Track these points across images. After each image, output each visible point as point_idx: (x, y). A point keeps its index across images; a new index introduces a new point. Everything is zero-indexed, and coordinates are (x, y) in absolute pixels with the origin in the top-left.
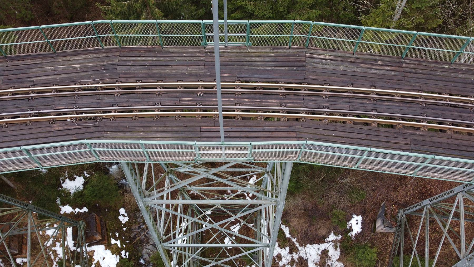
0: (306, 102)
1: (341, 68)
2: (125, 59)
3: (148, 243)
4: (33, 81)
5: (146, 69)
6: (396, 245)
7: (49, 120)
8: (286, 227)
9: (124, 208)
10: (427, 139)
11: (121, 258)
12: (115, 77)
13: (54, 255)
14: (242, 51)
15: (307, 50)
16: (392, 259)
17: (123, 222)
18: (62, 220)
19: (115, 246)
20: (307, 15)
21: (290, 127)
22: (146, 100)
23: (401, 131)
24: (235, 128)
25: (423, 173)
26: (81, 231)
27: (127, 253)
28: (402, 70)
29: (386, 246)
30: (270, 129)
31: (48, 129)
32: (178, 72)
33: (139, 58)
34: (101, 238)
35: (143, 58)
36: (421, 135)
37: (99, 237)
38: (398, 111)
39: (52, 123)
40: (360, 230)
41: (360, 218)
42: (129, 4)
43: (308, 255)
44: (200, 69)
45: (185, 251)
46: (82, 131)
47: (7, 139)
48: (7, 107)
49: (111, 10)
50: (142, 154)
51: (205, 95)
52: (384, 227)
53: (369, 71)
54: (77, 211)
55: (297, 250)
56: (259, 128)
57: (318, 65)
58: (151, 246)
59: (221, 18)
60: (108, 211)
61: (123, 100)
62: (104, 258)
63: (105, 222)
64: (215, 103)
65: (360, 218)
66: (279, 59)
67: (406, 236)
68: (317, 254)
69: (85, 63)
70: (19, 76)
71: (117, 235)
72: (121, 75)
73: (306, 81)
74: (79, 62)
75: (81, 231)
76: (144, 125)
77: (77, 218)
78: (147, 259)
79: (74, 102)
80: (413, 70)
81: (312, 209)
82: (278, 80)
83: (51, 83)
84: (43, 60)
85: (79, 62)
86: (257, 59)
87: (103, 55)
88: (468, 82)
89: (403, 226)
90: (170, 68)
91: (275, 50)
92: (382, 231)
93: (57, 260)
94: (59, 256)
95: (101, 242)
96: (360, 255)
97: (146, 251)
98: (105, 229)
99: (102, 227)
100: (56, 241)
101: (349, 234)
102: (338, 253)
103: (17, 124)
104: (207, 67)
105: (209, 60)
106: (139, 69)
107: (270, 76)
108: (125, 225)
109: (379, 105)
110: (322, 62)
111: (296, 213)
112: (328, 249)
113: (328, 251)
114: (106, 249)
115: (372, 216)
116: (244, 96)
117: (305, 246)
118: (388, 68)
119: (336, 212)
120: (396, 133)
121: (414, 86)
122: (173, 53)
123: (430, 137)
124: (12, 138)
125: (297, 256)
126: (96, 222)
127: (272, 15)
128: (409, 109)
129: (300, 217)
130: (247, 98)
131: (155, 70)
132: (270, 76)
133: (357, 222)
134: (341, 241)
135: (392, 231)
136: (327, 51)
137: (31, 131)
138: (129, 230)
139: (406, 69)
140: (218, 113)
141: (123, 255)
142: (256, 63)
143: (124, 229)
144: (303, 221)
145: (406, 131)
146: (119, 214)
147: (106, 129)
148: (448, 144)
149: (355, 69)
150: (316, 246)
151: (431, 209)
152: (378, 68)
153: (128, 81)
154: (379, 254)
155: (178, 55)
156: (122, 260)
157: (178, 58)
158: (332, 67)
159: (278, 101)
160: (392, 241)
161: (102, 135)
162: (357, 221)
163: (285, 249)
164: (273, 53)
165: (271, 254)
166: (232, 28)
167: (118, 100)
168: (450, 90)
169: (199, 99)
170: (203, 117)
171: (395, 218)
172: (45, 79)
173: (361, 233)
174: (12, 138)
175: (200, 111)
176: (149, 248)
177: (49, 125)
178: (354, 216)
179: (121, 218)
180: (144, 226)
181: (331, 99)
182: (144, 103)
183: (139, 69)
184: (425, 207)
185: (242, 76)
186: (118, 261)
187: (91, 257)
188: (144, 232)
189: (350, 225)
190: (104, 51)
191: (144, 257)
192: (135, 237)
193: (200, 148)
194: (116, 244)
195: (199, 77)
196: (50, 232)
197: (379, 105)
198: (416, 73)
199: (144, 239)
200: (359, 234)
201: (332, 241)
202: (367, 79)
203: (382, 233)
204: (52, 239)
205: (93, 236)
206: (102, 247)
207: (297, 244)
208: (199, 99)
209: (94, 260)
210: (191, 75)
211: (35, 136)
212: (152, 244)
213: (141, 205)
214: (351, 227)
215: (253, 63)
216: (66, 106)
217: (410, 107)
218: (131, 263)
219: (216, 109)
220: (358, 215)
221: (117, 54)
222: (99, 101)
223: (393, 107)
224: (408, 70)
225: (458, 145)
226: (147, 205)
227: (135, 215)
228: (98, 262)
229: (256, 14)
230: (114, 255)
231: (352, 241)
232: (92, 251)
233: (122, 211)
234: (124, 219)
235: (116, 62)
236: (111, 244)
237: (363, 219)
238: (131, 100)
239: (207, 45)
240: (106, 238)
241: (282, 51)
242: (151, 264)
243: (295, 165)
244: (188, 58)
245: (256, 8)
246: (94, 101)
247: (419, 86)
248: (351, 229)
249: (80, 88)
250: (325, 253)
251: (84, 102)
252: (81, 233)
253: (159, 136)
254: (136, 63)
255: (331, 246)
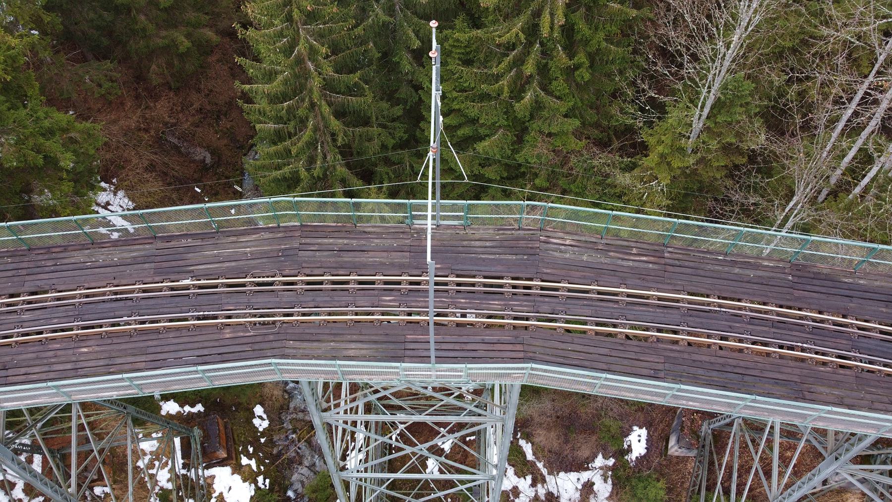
0: (537, 304)
1: (585, 258)
2: (308, 241)
3: (301, 464)
4: (192, 271)
5: (335, 256)
6: (697, 477)
7: (216, 325)
8: (527, 443)
9: (262, 405)
10: (686, 356)
11: (258, 489)
12: (296, 266)
13: (151, 483)
14: (458, 232)
15: (543, 233)
16: (691, 498)
17: (261, 429)
18: (170, 428)
19: (247, 469)
20: (559, 125)
21: (517, 337)
22: (336, 299)
23: (654, 345)
24: (448, 338)
25: (675, 402)
26: (196, 443)
27: (268, 481)
28: (663, 261)
29: (682, 478)
30: (493, 339)
31: (216, 337)
32: (375, 261)
33: (326, 241)
34: (226, 456)
35: (331, 241)
36: (678, 351)
37: (223, 454)
38: (652, 318)
39: (221, 329)
40: (643, 452)
41: (644, 432)
42: (289, 107)
43: (560, 490)
44: (404, 257)
45: (365, 482)
46: (259, 339)
47: (166, 349)
48: (163, 306)
49: (259, 110)
50: (336, 373)
51: (411, 294)
52: (680, 448)
53: (620, 262)
54: (187, 411)
55: (544, 481)
56: (478, 339)
57: (555, 253)
58: (306, 469)
59: (436, 284)
60: (236, 410)
61: (309, 299)
62: (230, 488)
63: (232, 429)
64: (423, 304)
65: (644, 432)
66: (506, 244)
67: (711, 463)
68: (577, 488)
69: (257, 246)
70: (174, 264)
71: (251, 450)
72: (304, 265)
73: (539, 275)
74: (249, 244)
75: (196, 443)
76: (335, 332)
77: (189, 423)
78: (300, 491)
79: (246, 300)
80: (677, 262)
81: (570, 415)
82: (503, 274)
83: (216, 274)
84: (202, 241)
85: (249, 244)
86: (478, 243)
87: (279, 235)
88: (745, 280)
89: (707, 448)
90: (365, 254)
91: (501, 232)
92: (676, 454)
93: (157, 491)
94: (160, 484)
95: (225, 462)
96: (639, 492)
97: (300, 476)
98: (232, 441)
99: (227, 437)
100: (155, 460)
101: (626, 457)
102: (609, 487)
103: (178, 329)
104: (412, 254)
105: (416, 244)
106: (327, 256)
107: (493, 269)
108: (263, 434)
109: (629, 309)
110: (560, 249)
111: (543, 422)
112: (593, 480)
113: (593, 484)
114: (233, 474)
115: (663, 430)
116: (459, 295)
117: (558, 474)
118: (644, 258)
119: (607, 421)
120: (648, 348)
121: (675, 285)
122: (369, 233)
123: (689, 353)
124: (172, 348)
125: (544, 492)
126: (219, 429)
127: (506, 123)
128: (667, 316)
129: (549, 429)
130: (463, 299)
131: (347, 258)
132: (493, 269)
133: (639, 438)
134: (613, 468)
135: (693, 453)
136: (567, 233)
137: (196, 339)
138: (271, 442)
139: (668, 261)
140: (428, 318)
141: (260, 484)
142: (475, 249)
143: (263, 440)
144: (553, 434)
145: (660, 345)
146: (253, 415)
147: (288, 337)
148: (711, 363)
149: (603, 260)
150: (573, 476)
151: (743, 425)
152: (632, 258)
153: (313, 273)
154: (669, 490)
155: (375, 236)
156: (259, 492)
157: (376, 241)
158: (573, 256)
159: (502, 303)
160: (691, 471)
161: (284, 345)
162: (639, 436)
163: (525, 479)
164: (498, 235)
165: (498, 487)
166: (444, 208)
167: (302, 299)
168: (720, 290)
169: (404, 299)
170: (408, 322)
171: (695, 434)
172: (208, 269)
173: (645, 455)
174: (172, 348)
175: (405, 315)
176: (302, 472)
177: (217, 331)
178: (635, 428)
179: (256, 422)
180: (294, 436)
181: (569, 301)
182: (335, 303)
183: (327, 256)
184: (736, 420)
185: (458, 268)
186: (253, 493)
187: (210, 485)
188: (296, 446)
189: (629, 444)
190: (281, 229)
191: (295, 487)
192: (280, 454)
193: (405, 370)
194: (249, 466)
195: (402, 269)
196: (148, 446)
197: (629, 309)
198: (680, 266)
199: (295, 457)
200: (641, 457)
201: (601, 468)
202: (617, 274)
203: (677, 457)
204: (149, 457)
205: (215, 452)
206: (227, 470)
207: (544, 471)
208: (404, 299)
209: (215, 492)
210: (392, 265)
211: (201, 345)
212: (307, 465)
213: (317, 422)
214: (630, 446)
215: (472, 249)
216: (236, 306)
217: (668, 313)
218: (274, 497)
219: (427, 314)
220: (641, 428)
221: (298, 234)
222: (278, 299)
223: (646, 313)
224: (671, 261)
225: (723, 365)
226: (325, 421)
227: (280, 418)
228: (221, 494)
229: (481, 121)
230: (247, 484)
231: (630, 468)
232: (211, 476)
233: (259, 410)
234: (261, 424)
235: (297, 245)
236: (241, 466)
237: (648, 433)
238: (318, 299)
239: (413, 224)
240: (234, 456)
241: (509, 232)
242: (306, 499)
243: (524, 387)
244: (389, 241)
245: (482, 113)
246: (271, 300)
247: (680, 285)
248: (629, 450)
249: (253, 282)
250: (588, 487)
251: (259, 300)
252: (196, 447)
253: (353, 347)
254: (324, 248)
255: (599, 476)
